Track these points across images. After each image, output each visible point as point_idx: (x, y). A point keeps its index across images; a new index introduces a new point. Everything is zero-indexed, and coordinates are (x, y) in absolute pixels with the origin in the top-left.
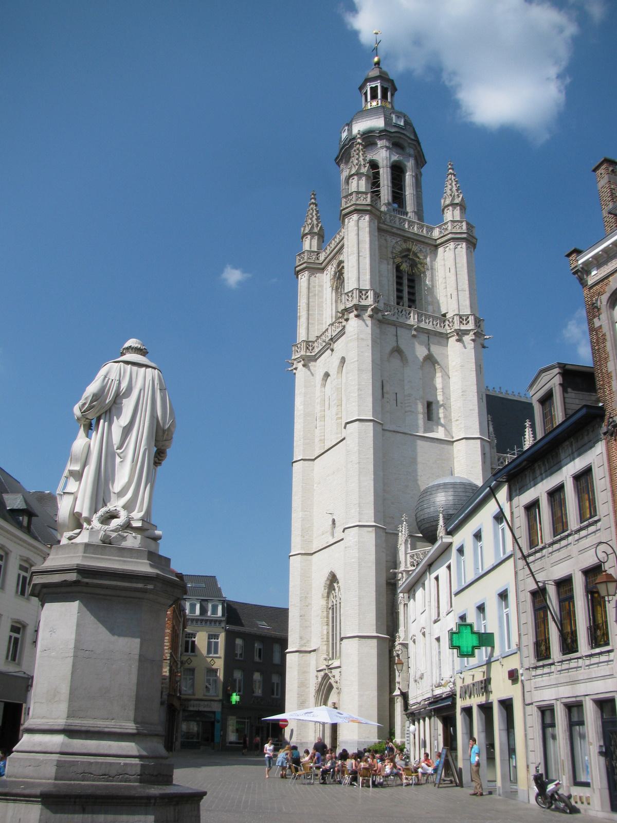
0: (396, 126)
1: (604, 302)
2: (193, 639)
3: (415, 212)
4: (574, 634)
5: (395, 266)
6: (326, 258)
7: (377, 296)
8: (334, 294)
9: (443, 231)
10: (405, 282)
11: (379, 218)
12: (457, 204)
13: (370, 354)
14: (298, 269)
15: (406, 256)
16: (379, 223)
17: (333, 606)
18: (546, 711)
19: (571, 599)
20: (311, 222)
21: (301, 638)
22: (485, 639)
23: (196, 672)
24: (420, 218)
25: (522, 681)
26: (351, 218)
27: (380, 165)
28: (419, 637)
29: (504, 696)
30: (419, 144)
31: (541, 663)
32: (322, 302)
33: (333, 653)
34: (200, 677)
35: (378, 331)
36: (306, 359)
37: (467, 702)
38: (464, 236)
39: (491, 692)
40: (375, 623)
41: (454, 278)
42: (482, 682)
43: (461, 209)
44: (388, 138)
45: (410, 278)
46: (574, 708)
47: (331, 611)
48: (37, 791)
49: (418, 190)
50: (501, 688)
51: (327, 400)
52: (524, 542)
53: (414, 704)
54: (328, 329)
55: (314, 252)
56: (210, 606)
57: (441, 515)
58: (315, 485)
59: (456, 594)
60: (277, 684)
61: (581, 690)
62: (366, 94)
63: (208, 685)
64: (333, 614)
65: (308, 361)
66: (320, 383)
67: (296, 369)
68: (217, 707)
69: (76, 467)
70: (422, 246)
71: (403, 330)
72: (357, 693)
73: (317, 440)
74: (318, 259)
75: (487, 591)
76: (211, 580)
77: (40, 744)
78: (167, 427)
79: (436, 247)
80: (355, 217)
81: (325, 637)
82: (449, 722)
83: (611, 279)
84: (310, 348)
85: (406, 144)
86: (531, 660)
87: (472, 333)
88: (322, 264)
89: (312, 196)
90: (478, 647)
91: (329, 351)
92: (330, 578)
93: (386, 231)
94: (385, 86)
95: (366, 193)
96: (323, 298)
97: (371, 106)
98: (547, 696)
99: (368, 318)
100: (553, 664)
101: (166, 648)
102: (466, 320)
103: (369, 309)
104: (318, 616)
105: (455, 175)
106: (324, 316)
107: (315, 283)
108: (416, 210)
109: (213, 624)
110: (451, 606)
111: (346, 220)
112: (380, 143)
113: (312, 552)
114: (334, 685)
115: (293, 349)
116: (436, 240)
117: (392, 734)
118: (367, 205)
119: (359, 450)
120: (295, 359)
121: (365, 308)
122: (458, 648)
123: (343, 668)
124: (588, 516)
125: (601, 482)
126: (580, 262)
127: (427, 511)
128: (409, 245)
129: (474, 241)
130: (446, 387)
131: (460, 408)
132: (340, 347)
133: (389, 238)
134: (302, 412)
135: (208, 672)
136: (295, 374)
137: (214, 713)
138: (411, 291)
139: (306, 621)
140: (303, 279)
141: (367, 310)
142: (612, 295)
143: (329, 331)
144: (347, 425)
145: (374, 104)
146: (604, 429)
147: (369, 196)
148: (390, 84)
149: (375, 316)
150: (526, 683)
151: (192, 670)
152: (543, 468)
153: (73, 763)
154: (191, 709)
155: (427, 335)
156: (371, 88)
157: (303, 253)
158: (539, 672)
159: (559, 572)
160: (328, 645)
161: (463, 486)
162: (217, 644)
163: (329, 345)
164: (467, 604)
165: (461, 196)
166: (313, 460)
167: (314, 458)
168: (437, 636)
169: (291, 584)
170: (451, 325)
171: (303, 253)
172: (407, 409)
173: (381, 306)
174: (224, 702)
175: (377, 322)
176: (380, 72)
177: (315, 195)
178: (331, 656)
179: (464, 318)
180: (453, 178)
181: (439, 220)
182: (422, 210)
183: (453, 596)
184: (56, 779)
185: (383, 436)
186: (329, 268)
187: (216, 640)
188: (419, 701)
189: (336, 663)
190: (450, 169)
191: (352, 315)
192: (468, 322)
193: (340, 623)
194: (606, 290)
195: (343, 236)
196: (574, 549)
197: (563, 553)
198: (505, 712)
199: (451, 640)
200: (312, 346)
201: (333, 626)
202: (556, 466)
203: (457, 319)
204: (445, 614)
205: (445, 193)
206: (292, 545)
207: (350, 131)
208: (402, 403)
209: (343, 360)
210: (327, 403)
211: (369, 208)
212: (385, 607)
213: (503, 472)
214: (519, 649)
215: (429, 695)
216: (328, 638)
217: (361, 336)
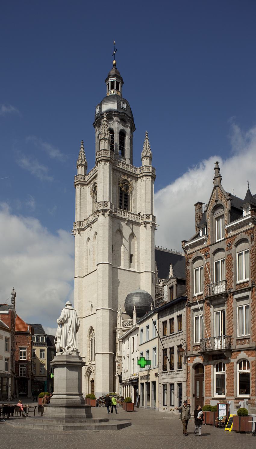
0: (123, 109)
1: (191, 262)
2: (34, 352)
3: (129, 159)
4: (173, 364)
6: (88, 180)
7: (111, 205)
8: (92, 199)
9: (141, 171)
10: (124, 196)
12: (148, 156)
14: (75, 184)
16: (113, 166)
17: (91, 340)
18: (165, 385)
19: (173, 353)
20: (81, 158)
22: (149, 362)
24: (131, 162)
25: (159, 376)
26: (101, 163)
27: (115, 132)
28: (126, 357)
29: (154, 380)
30: (133, 120)
31: (164, 372)
33: (92, 358)
34: (38, 367)
35: (111, 222)
37: (142, 381)
38: (151, 174)
39: (150, 379)
41: (144, 196)
42: (147, 376)
43: (150, 159)
44: (119, 115)
45: (126, 194)
46: (172, 385)
47: (91, 342)
49: (131, 145)
50: (152, 378)
51: (89, 250)
52: (161, 334)
53: (124, 380)
54: (89, 217)
55: (83, 175)
56: (40, 337)
57: (135, 307)
58: (84, 289)
59: (140, 345)
61: (174, 380)
62: (108, 85)
63: (41, 371)
64: (92, 343)
65: (80, 231)
66: (86, 242)
67: (75, 234)
68: (45, 379)
72: (102, 375)
73: (84, 268)
75: (150, 346)
77: (61, 397)
78: (78, 325)
79: (138, 178)
80: (103, 163)
81: (89, 352)
82: (136, 387)
83: (194, 254)
84: (81, 225)
85: (127, 120)
86: (162, 371)
87: (151, 223)
88: (86, 182)
89: (82, 143)
90: (146, 365)
91: (90, 228)
93: (116, 170)
95: (108, 151)
96: (87, 200)
97: (111, 93)
98: (165, 381)
99: (108, 216)
100: (167, 372)
101: (29, 357)
102: (149, 217)
103: (108, 211)
104: (85, 344)
105: (148, 140)
106: (87, 209)
107: (83, 192)
108: (129, 158)
109: (40, 345)
110: (138, 349)
111: (99, 164)
113: (83, 317)
114: (92, 371)
115: (74, 224)
116: (138, 175)
117: (114, 391)
118: (108, 157)
119: (103, 276)
120: (74, 230)
121: (106, 211)
122: (140, 365)
123: (97, 365)
124: (180, 329)
125: (184, 318)
126: (185, 245)
127: (129, 304)
129: (155, 177)
130: (139, 248)
131: (144, 258)
132: (95, 227)
134: (78, 255)
135: (41, 365)
136: (74, 236)
137: (44, 381)
138: (126, 201)
139: (81, 346)
140: (78, 189)
141: (107, 212)
142: (193, 259)
143: (90, 218)
144: (98, 265)
146: (186, 304)
147: (109, 152)
149: (110, 215)
150: (159, 377)
151: (35, 364)
152: (170, 310)
153: (69, 400)
156: (111, 82)
157: (78, 175)
158: (163, 374)
159: (171, 345)
160: (90, 355)
161: (143, 294)
162: (44, 354)
163: (89, 225)
164: (143, 349)
165: (150, 152)
166: (83, 277)
167: (83, 276)
168: (133, 358)
170: (142, 219)
171: (78, 175)
174: (48, 377)
175: (111, 218)
176: (116, 72)
177: (83, 143)
178: (91, 360)
179: (148, 216)
180: (148, 141)
181: (140, 165)
182: (132, 157)
183: (130, 269)
184: (66, 403)
186: (90, 184)
187: (43, 352)
188: (126, 379)
189: (93, 363)
190: (147, 136)
191: (101, 214)
193: (95, 347)
194: (192, 257)
195: (96, 170)
196: (175, 339)
197: (172, 340)
198: (153, 386)
199: (138, 362)
200: (82, 224)
201: (92, 348)
202: (172, 312)
203: (145, 216)
204: (136, 351)
205: (144, 149)
207: (101, 109)
209: (96, 233)
210: (89, 252)
211: (109, 159)
212: (112, 342)
213: (157, 310)
214: (158, 366)
215: (130, 378)
216: (90, 353)
217: (104, 224)
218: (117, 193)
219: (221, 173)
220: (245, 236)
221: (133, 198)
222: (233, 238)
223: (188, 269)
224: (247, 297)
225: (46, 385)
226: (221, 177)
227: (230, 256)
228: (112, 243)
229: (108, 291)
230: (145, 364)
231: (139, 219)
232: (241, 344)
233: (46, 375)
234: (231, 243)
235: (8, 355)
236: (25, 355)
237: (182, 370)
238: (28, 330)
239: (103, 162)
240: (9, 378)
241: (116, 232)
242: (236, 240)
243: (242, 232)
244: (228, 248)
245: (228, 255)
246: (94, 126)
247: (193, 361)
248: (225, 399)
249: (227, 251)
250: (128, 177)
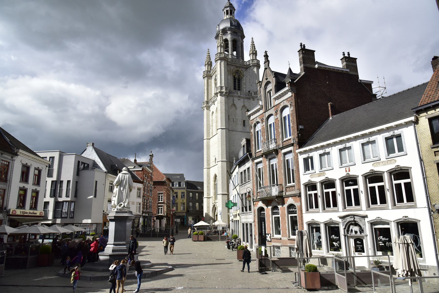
1: (253, 126)
10: (237, 81)
15: (237, 72)
32: (212, 88)
40: (226, 190)
69: (114, 195)
70: (242, 68)
74: (210, 73)
76: (182, 175)
84: (208, 103)
85: (238, 32)
91: (213, 105)
92: (215, 176)
94: (231, 9)
101: (165, 200)
102: (256, 93)
111: (217, 62)
112: (229, 32)
121: (223, 92)
137: (184, 216)
138: (239, 84)
144: (218, 130)
145: (227, 16)
148: (233, 9)
149: (226, 95)
154: (177, 215)
156: (227, 10)
169: (204, 177)
170: (251, 95)
172: (237, 123)
173: (228, 91)
185: (229, 132)
192: (257, 94)
218: (232, 80)
220: (286, 103)
222: (278, 106)
227: (277, 120)
228: (228, 113)
229: (225, 148)
230: (232, 206)
231: (248, 95)
233: (186, 211)
234: (277, 110)
235: (140, 200)
236: (162, 198)
237: (251, 212)
238: (165, 179)
239: (219, 61)
240: (140, 218)
241: (231, 106)
242: (281, 107)
243: (284, 101)
244: (276, 113)
245: (276, 119)
247: (258, 205)
248: (281, 239)
249: (275, 115)
250: (239, 68)
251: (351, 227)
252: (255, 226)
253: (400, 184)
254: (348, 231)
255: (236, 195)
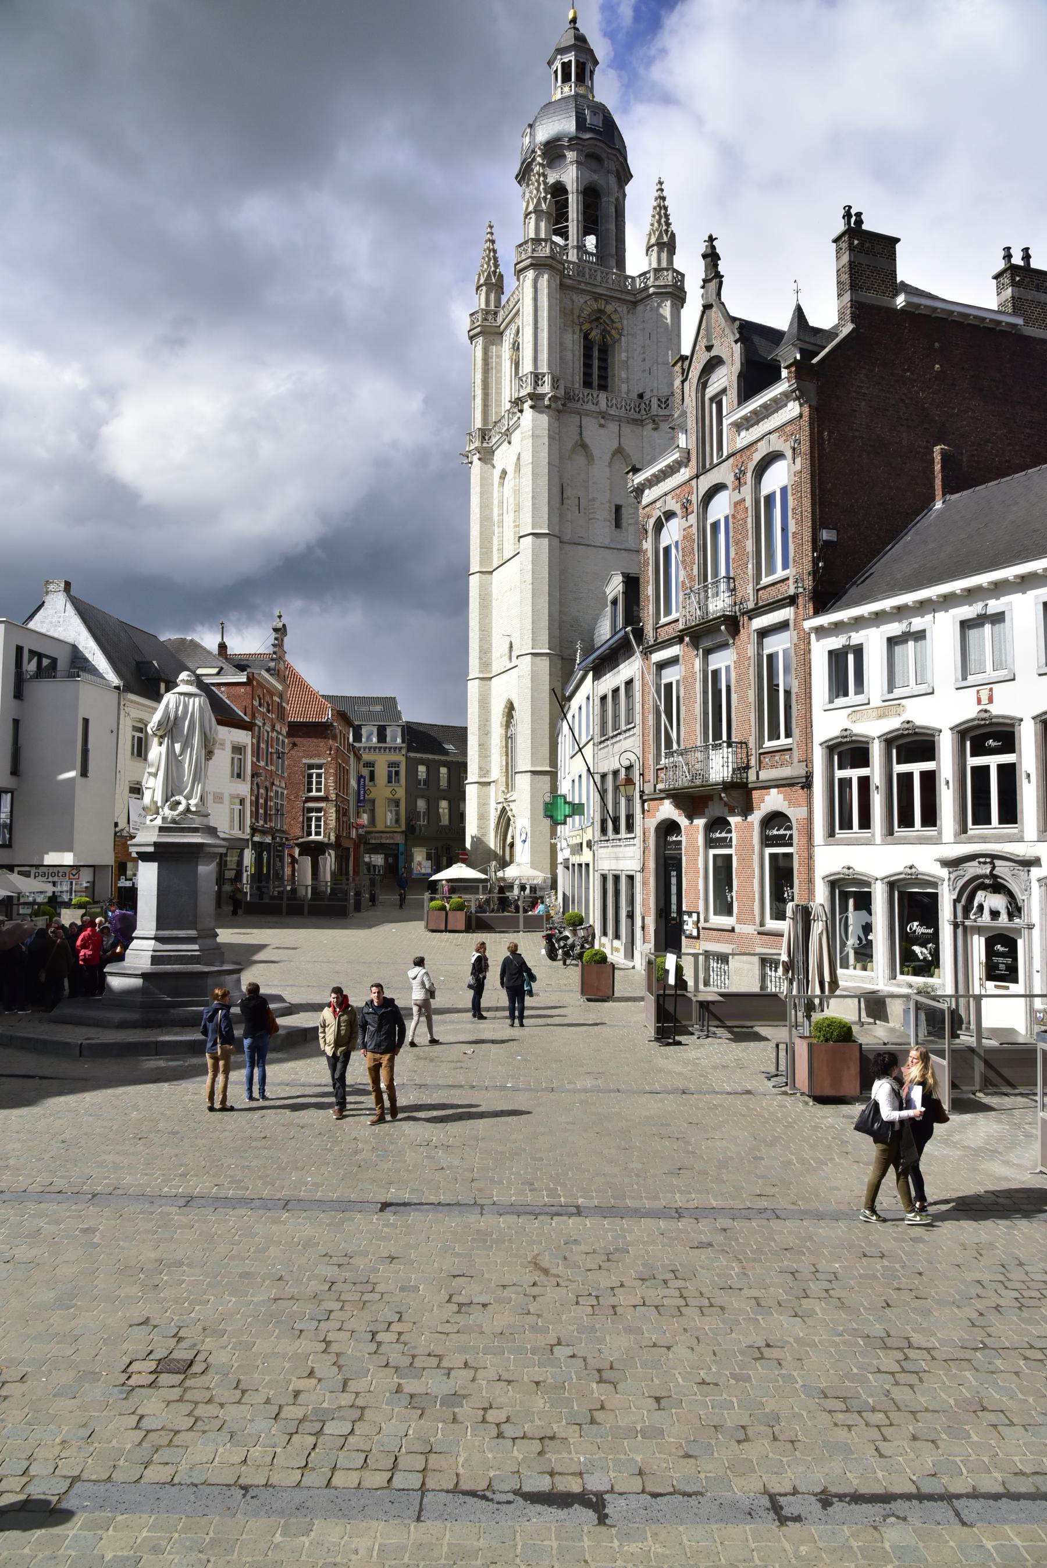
5: (582, 335)
7: (555, 383)
10: (596, 354)
11: (561, 273)
13: (547, 455)
21: (480, 768)
23: (376, 802)
27: (569, 188)
32: (501, 377)
36: (482, 451)
44: (580, 147)
48: (139, 972)
60: (728, 668)
62: (556, 72)
69: (153, 770)
70: (618, 304)
71: (588, 419)
76: (390, 703)
85: (604, 156)
94: (582, 60)
97: (562, 93)
102: (665, 402)
112: (571, 156)
128: (601, 304)
133: (575, 297)
155: (618, 423)
156: (563, 64)
172: (591, 516)
173: (561, 393)
185: (561, 549)
203: (654, 402)
206: (470, 668)
208: (585, 509)
218: (576, 347)
219: (722, 268)
220: (777, 443)
221: (569, 355)
222: (748, 453)
223: (644, 547)
224: (783, 626)
225: (402, 854)
226: (723, 276)
227: (742, 506)
232: (772, 767)
234: (743, 468)
236: (319, 783)
239: (531, 271)
241: (574, 449)
242: (757, 457)
243: (770, 433)
246: (519, 182)
248: (733, 930)
250: (607, 303)
251: (980, 896)
252: (645, 883)
253: (910, 775)
254: (967, 910)
255: (580, 776)
